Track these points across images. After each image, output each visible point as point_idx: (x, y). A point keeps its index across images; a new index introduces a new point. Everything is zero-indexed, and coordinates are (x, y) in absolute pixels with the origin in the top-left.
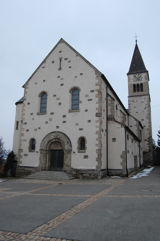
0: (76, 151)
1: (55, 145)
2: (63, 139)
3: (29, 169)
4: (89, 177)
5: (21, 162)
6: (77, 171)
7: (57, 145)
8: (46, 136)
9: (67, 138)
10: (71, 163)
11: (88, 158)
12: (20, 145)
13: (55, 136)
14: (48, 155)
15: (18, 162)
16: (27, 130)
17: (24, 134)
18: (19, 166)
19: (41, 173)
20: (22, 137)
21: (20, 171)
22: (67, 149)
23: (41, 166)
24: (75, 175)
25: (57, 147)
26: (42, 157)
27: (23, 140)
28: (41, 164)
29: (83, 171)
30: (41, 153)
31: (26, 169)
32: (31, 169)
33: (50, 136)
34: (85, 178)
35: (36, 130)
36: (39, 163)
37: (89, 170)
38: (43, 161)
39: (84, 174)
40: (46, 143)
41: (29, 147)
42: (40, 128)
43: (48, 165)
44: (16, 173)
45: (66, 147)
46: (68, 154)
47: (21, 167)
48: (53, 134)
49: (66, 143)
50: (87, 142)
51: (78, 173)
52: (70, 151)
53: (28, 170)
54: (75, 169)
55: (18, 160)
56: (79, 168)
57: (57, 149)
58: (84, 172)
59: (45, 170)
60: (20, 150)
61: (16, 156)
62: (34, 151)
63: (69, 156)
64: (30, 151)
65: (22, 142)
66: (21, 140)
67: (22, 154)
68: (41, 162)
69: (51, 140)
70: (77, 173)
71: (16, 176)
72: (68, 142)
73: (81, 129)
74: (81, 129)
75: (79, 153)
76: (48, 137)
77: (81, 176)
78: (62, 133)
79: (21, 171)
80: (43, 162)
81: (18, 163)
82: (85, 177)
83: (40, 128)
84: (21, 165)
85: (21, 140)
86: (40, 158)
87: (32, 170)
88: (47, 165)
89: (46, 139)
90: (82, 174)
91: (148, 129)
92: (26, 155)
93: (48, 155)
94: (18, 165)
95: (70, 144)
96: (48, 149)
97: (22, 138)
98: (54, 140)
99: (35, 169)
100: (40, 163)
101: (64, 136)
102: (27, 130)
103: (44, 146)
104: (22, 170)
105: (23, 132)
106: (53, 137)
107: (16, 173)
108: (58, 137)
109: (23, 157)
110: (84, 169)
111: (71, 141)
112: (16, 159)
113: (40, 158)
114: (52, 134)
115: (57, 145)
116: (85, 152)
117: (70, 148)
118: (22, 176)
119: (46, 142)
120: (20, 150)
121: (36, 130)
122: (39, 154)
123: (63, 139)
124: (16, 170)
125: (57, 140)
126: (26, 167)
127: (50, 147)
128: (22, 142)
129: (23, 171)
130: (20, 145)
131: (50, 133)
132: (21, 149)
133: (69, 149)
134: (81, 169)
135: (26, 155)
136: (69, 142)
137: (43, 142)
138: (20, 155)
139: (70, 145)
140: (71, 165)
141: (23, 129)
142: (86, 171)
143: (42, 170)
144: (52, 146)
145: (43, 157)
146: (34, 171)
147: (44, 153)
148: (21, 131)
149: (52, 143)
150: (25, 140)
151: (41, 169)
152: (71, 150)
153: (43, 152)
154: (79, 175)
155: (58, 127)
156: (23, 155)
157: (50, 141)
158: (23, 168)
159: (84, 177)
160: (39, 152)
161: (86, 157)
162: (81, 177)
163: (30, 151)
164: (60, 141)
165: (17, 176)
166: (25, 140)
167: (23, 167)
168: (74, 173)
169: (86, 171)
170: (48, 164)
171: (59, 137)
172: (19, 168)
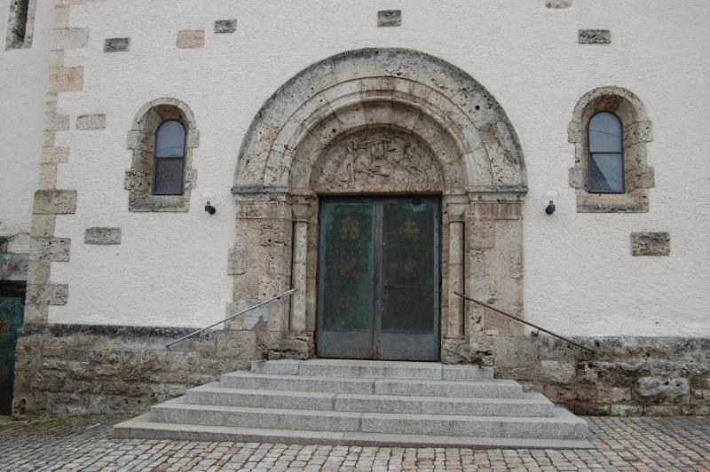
0: (567, 199)
1: (364, 159)
2: (444, 103)
3: (137, 346)
4: (687, 400)
5: (62, 296)
6: (585, 353)
7: (374, 158)
8: (291, 82)
9: (478, 99)
10: (520, 293)
11: (667, 253)
12: (52, 157)
13: (375, 84)
14: (302, 231)
15: (30, 292)
16: (115, 45)
17: (87, 73)
18: (40, 328)
19: (265, 383)
20: (61, 95)
21: (54, 362)
22: (488, 182)
23: (251, 322)
24: (562, 385)
25: (376, 172)
26: (258, 253)
27: (73, 121)
28: (243, 306)
29: (631, 353)
30: (245, 217)
31: (109, 345)
32: (159, 346)
33: (328, 81)
34: (660, 409)
35: (190, 39)
36: (228, 297)
37: (687, 345)
38: (265, 279)
39: (646, 380)
40: (290, 135)
41: (130, 174)
42: (226, 26)
43: (303, 306)
44: (20, 379)
45: (478, 167)
46: (498, 225)
47: (59, 330)
48: (347, 70)
49: (471, 136)
50: (655, 127)
51: (591, 374)
52: (510, 200)
53: (131, 354)
54: (560, 340)
55: (31, 278)
56: (594, 329)
57: (375, 186)
58: (639, 362)
59: (285, 352)
60: (51, 199)
61: (13, 247)
62: (181, 207)
63: (502, 236)
64: (135, 205)
65: (61, 138)
66: (57, 121)
67: (65, 227)
68: (245, 291)
69: (334, 115)
70: (579, 367)
71: (15, 401)
72: (489, 130)
73: (593, 37)
74: (593, 37)
75: (591, 216)
76: (303, 89)
77: (618, 393)
78: (433, 59)
79: (62, 369)
80: (268, 289)
81: (34, 300)
82: (659, 399)
83: (226, 26)
84: (56, 315)
85: (57, 121)
86: (238, 261)
87: (162, 356)
88: (299, 312)
89: (289, 106)
90: (630, 378)
91: (489, 130)
92: (100, 236)
93: (302, 231)
94: (31, 314)
95: (508, 145)
96: (302, 187)
97: (69, 103)
98: (358, 120)
99: (192, 348)
100: (237, 296)
101: (452, 84)
102: (115, 45)
103: (275, 160)
104: (77, 354)
105: (72, 57)
106: (355, 87)
107: (12, 377)
108: (402, 87)
109: (78, 248)
110: (641, 340)
111: (512, 120)
112: (14, 268)
113: (233, 255)
114: (340, 66)
115: (374, 158)
116: (640, 207)
117: (510, 176)
118: (72, 401)
119: (293, 126)
120: (51, 199)
121: (190, 39)
122: (224, 233)
123: (448, 106)
124: (13, 361)
125: (383, 116)
126: (112, 331)
127: (318, 168)
128: (61, 138)
129: (76, 366)
130: (52, 157)
131: (323, 62)
132: (59, 192)
133: (506, 181)
134: (616, 343)
135: (100, 236)
136: (500, 126)
137: (262, 130)
138: (50, 240)
139: (507, 154)
140: (520, 305)
141: (79, 35)
142: (663, 354)
143: (266, 357)
144: (329, 167)
145: (268, 244)
146: (180, 360)
147: (272, 216)
148: (55, 94)
149: (341, 139)
150: (95, 121)
151: (250, 347)
152: (522, 191)
153: (262, 205)
154: (600, 386)
155: (390, 18)
156: (77, 239)
157: (321, 124)
158: (83, 338)
159: (644, 401)
160: (228, 208)
161: (652, 244)
162: (623, 401)
163: (135, 205)
164: (410, 123)
165: (28, 406)
166: (95, 121)
167: (76, 329)
168: (563, 370)
169: (663, 354)
170: (307, 304)
171: (411, 95)
172: (46, 337)
